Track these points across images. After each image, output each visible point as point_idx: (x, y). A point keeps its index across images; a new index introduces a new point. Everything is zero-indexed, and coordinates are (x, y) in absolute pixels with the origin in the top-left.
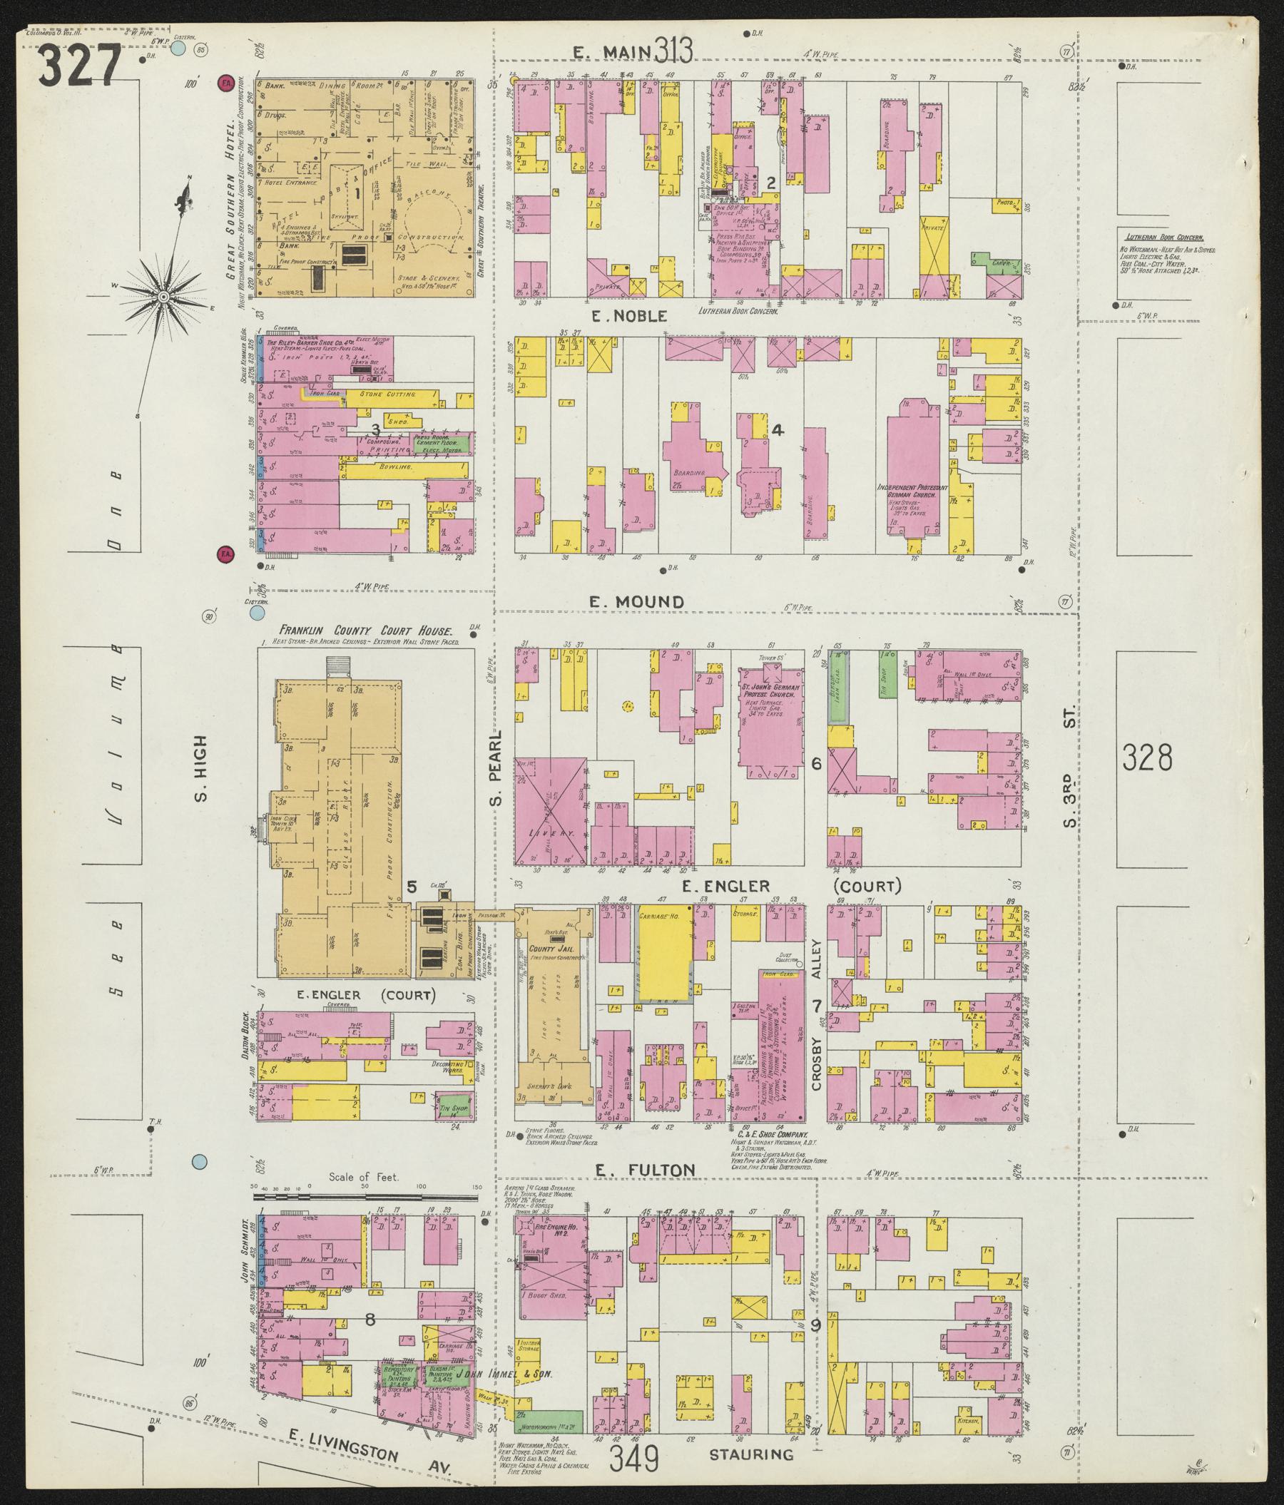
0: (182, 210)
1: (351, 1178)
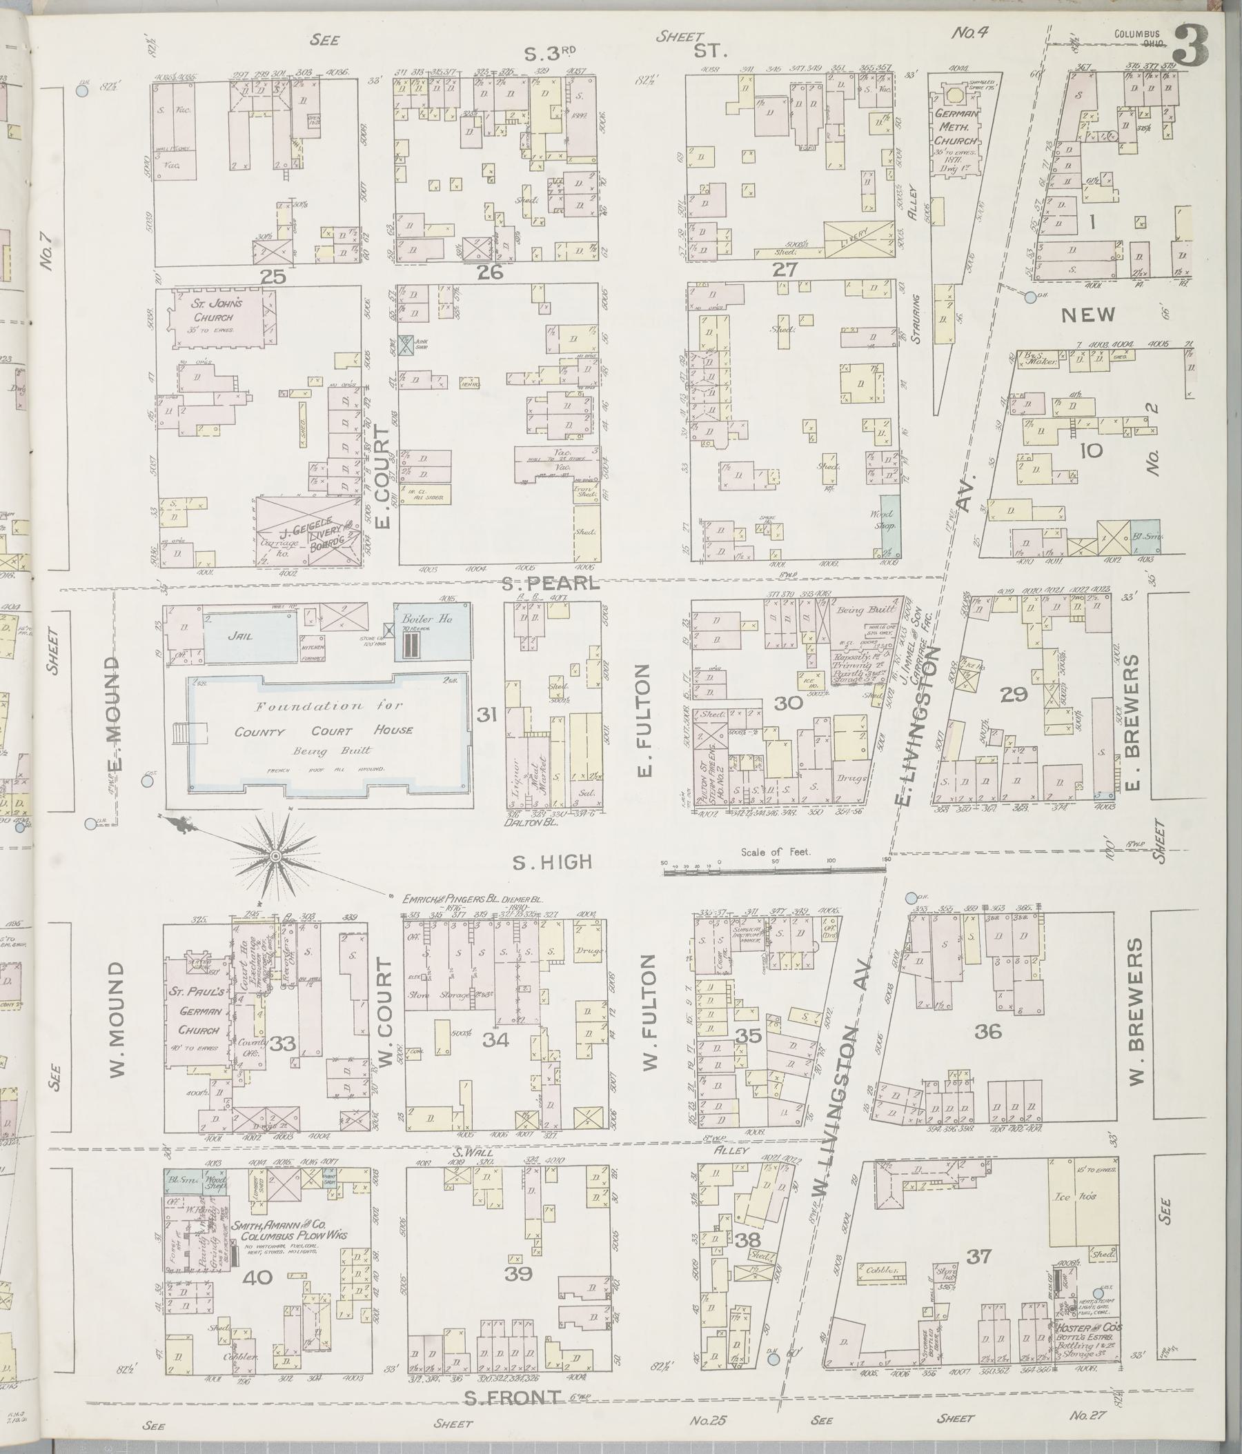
0: (191, 828)
1: (763, 853)
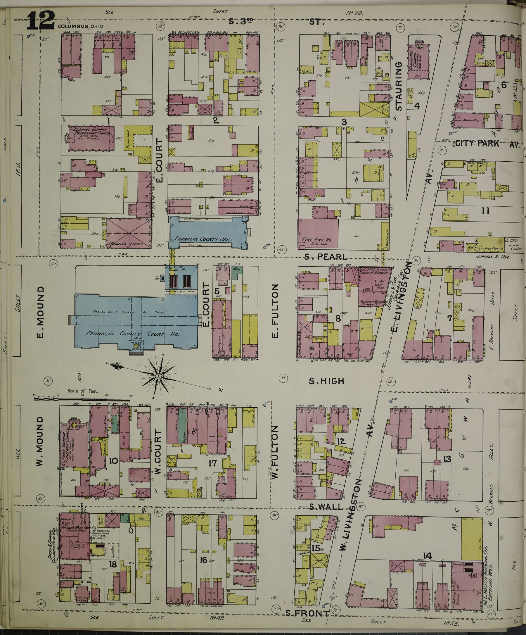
0: (121, 367)
1: (77, 391)
